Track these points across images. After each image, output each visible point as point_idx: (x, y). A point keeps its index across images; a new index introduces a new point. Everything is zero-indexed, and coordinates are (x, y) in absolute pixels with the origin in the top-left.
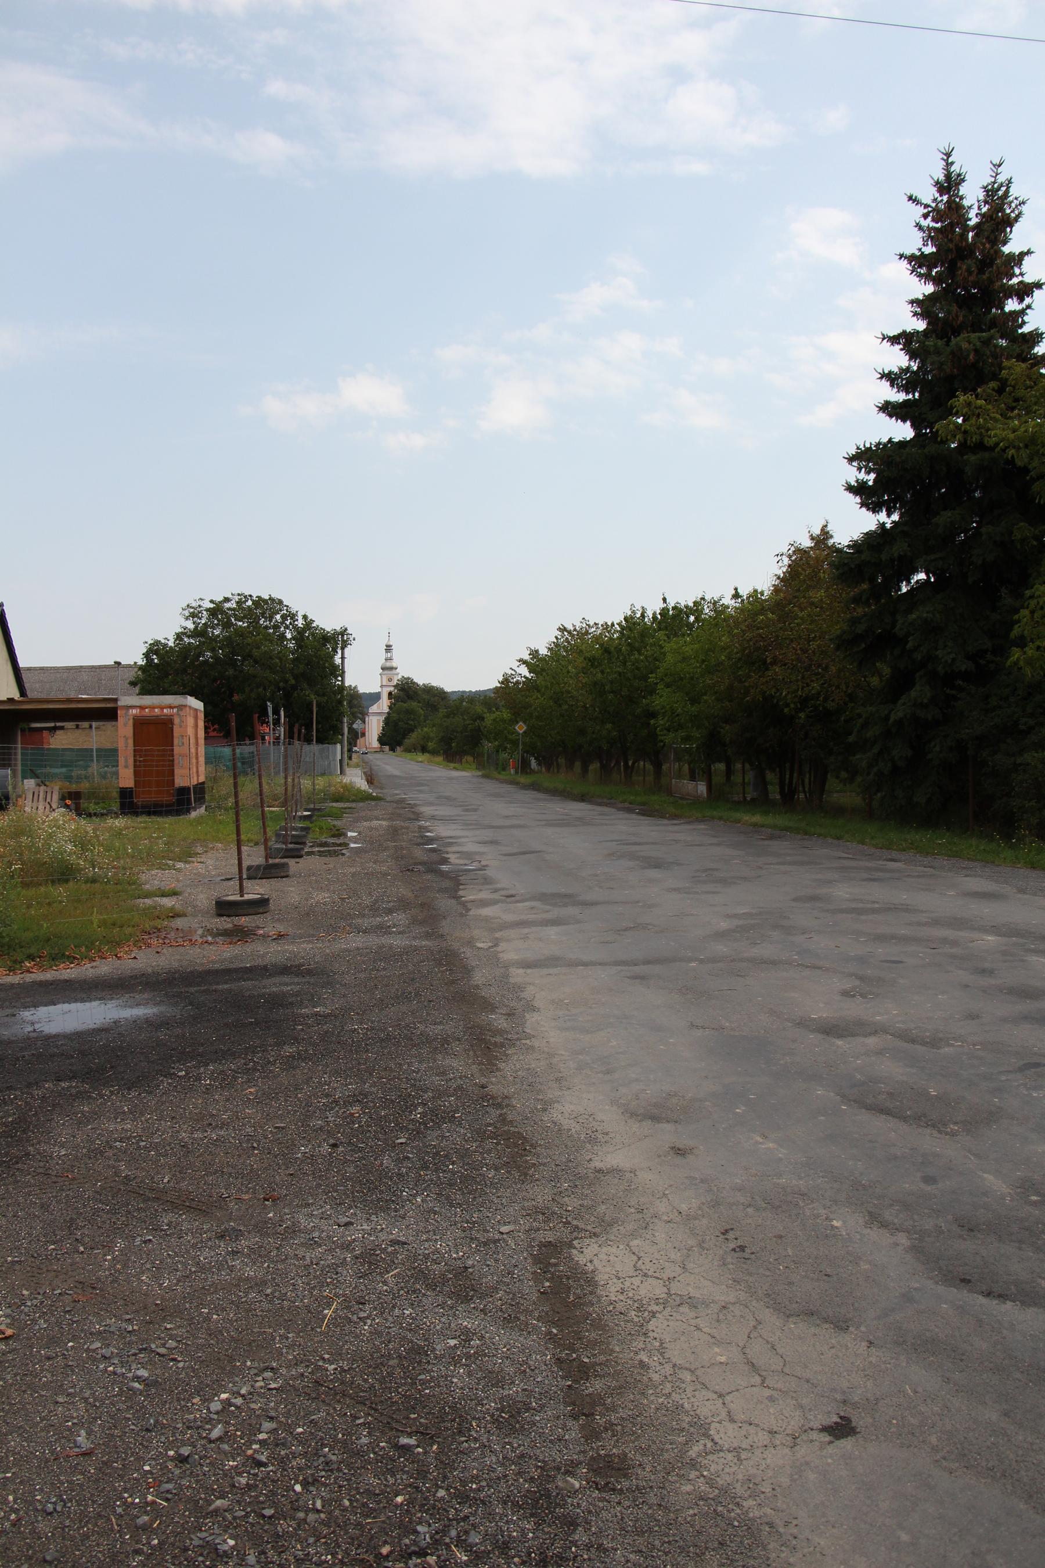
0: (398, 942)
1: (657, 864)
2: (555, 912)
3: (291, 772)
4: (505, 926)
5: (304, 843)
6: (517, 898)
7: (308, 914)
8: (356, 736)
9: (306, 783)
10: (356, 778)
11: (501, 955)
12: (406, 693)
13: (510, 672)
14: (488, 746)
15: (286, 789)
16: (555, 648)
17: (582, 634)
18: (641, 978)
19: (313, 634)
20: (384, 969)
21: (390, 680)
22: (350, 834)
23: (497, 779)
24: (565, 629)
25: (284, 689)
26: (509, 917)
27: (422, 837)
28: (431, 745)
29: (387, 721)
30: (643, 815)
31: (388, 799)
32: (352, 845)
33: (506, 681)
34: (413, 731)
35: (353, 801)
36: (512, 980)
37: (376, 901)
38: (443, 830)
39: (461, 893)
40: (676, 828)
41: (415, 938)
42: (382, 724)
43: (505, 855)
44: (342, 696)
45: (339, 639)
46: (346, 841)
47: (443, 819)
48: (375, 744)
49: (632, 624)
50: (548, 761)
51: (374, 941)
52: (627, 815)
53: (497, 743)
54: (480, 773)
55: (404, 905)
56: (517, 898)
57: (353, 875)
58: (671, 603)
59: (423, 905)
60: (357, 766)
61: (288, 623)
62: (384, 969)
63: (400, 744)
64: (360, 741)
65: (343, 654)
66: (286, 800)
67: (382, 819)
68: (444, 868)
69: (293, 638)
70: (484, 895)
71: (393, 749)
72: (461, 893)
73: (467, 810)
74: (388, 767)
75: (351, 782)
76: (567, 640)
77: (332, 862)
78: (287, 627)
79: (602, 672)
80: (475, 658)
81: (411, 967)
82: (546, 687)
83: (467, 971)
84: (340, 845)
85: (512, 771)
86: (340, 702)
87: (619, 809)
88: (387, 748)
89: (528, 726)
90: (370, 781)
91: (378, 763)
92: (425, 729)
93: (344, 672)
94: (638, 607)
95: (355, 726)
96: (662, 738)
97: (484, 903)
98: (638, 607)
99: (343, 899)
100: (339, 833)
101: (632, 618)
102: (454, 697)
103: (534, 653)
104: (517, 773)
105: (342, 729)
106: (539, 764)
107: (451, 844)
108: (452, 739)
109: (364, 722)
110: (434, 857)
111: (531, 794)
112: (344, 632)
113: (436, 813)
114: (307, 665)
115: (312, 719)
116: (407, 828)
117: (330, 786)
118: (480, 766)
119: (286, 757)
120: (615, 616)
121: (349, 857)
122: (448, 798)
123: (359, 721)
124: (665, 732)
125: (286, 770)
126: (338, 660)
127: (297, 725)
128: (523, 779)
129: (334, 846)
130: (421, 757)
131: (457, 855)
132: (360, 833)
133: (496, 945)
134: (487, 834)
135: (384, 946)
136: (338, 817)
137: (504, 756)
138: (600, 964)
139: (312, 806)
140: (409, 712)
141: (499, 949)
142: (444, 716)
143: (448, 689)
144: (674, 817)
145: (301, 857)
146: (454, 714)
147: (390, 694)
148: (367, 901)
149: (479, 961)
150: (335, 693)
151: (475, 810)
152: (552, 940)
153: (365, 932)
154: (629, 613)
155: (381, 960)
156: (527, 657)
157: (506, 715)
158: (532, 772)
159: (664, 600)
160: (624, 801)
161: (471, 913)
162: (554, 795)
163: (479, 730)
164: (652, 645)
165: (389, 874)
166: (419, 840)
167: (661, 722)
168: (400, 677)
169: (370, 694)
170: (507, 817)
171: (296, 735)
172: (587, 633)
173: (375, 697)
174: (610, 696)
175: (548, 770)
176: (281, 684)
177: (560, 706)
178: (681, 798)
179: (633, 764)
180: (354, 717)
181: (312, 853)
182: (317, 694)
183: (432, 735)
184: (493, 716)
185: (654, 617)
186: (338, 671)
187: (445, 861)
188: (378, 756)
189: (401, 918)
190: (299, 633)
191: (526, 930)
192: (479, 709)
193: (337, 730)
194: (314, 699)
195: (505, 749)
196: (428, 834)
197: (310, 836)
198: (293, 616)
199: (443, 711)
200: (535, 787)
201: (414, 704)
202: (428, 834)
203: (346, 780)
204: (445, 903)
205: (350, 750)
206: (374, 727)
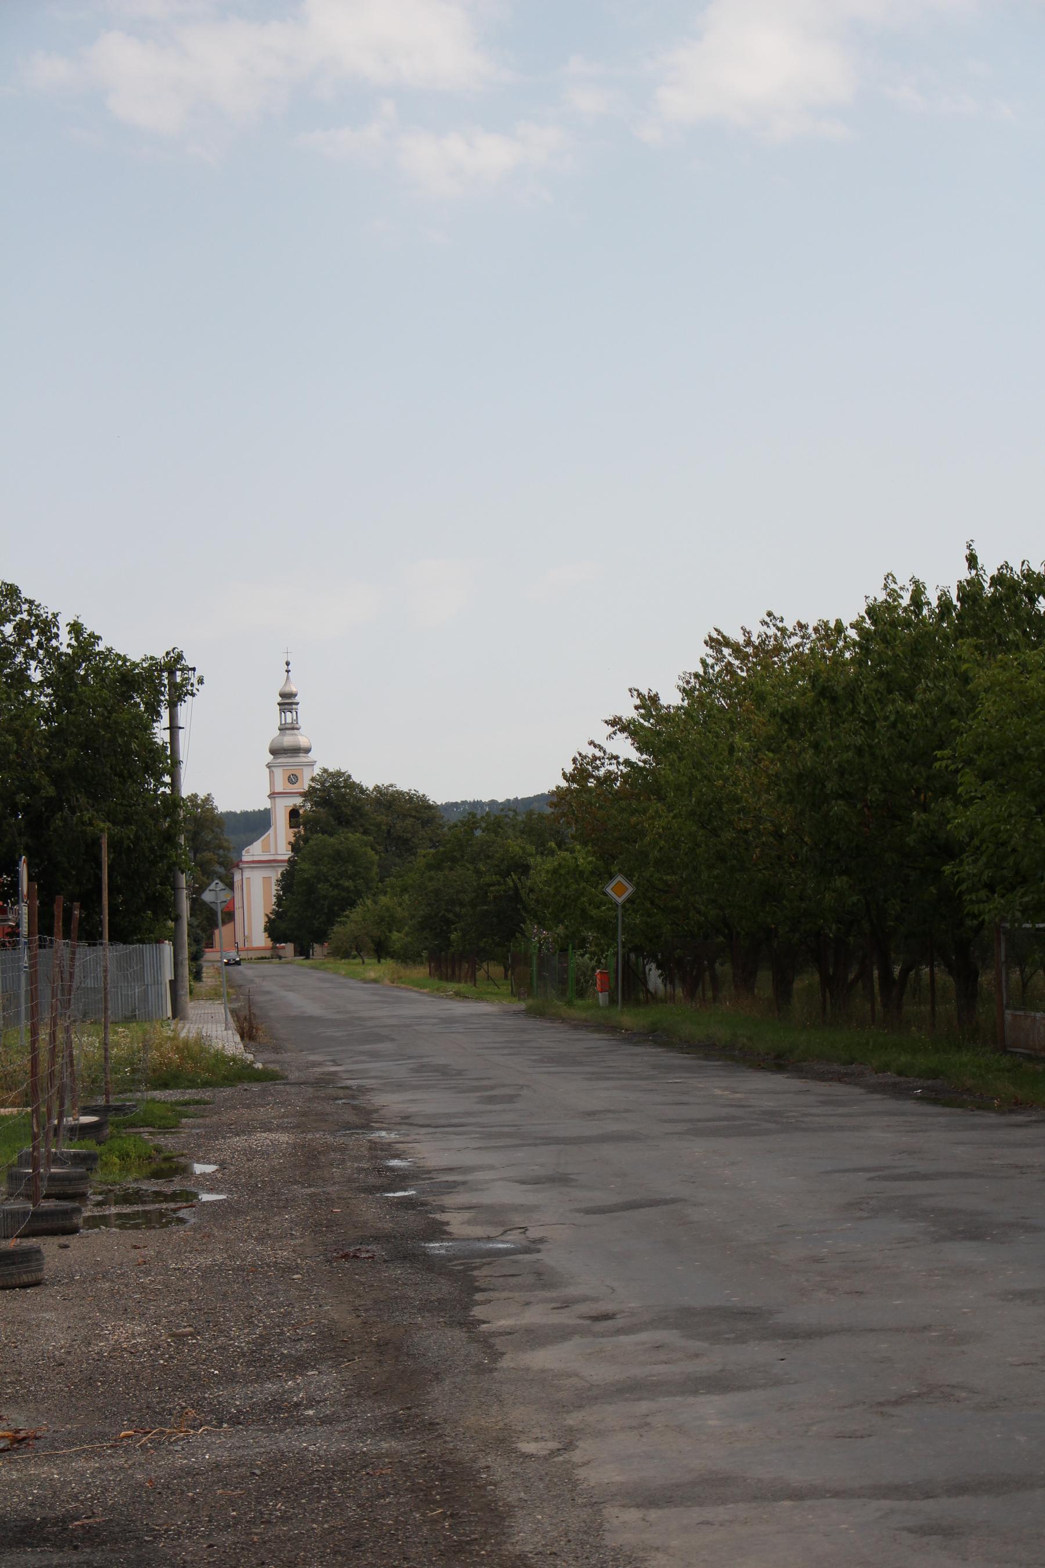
0: (317, 1444)
1: (973, 1229)
2: (716, 1358)
3: (47, 1017)
4: (590, 1396)
5: (82, 1197)
6: (620, 1322)
7: (90, 1381)
8: (209, 921)
9: (86, 1043)
10: (212, 1027)
11: (581, 1473)
12: (335, 811)
13: (590, 751)
14: (538, 936)
15: (34, 1062)
16: (701, 689)
17: (764, 653)
18: (946, 1531)
19: (97, 671)
20: (285, 1519)
21: (293, 779)
22: (199, 1168)
23: (563, 1020)
24: (727, 643)
25: (26, 808)
26: (600, 1373)
27: (381, 1170)
28: (397, 938)
29: (289, 882)
30: (935, 1101)
31: (294, 1076)
32: (206, 1197)
33: (580, 773)
34: (353, 904)
35: (206, 1084)
36: (611, 1540)
37: (265, 1339)
38: (430, 1153)
39: (478, 1312)
40: (1019, 1134)
41: (362, 1433)
42: (274, 889)
43: (588, 1211)
44: (175, 822)
45: (165, 681)
46: (189, 1186)
47: (436, 1125)
48: (260, 939)
49: (895, 632)
50: (688, 971)
51: (257, 1444)
52: (892, 1104)
53: (561, 930)
54: (522, 1006)
55: (333, 1346)
56: (620, 1322)
57: (207, 1273)
58: (990, 568)
59: (381, 1346)
60: (214, 995)
61: (33, 643)
62: (285, 1519)
63: (320, 937)
64: (222, 934)
65: (173, 717)
66: (34, 1088)
67: (281, 1128)
68: (435, 1247)
69: (47, 682)
70: (535, 1316)
71: (303, 951)
72: (478, 1312)
73: (491, 1100)
74: (292, 997)
75: (200, 1038)
76: (729, 668)
77: (151, 1240)
78: (31, 654)
79: (816, 746)
80: (503, 703)
81: (352, 1511)
82: (678, 788)
83: (497, 1516)
84: (173, 1197)
85: (602, 998)
86: (169, 838)
87: (873, 1089)
88: (289, 948)
89: (637, 885)
90: (248, 1033)
91: (268, 986)
92: (384, 900)
93: (176, 763)
94: (903, 580)
95: (207, 897)
96: (976, 909)
97: (536, 1337)
98: (903, 580)
99: (180, 1338)
100: (171, 1168)
101: (889, 608)
102: (454, 818)
103: (649, 703)
104: (613, 1001)
105: (176, 904)
106: (668, 978)
107: (451, 1187)
108: (448, 922)
109: (230, 885)
110: (410, 1220)
111: (649, 1055)
112: (174, 662)
113: (413, 1109)
114: (84, 747)
115: (99, 880)
116: (343, 1149)
117: (146, 1047)
118: (521, 988)
119: (32, 979)
120: (848, 609)
121: (196, 1229)
122: (443, 1071)
123: (217, 885)
124: (983, 893)
125: (34, 1013)
126: (161, 734)
127: (60, 899)
128: (628, 1018)
129: (158, 1199)
130: (374, 969)
131: (467, 1215)
132: (223, 1165)
133: (569, 1447)
134: (541, 1160)
135: (283, 1457)
136: (167, 1127)
137: (580, 960)
138: (836, 1494)
139: (101, 1101)
140: (340, 857)
141: (576, 1456)
142: (429, 867)
143: (438, 796)
144: (1015, 1105)
145: (73, 1231)
146: (454, 860)
147: (294, 813)
148: (242, 1340)
149: (527, 1489)
150: (154, 814)
151: (511, 1099)
152: (709, 1431)
153: (235, 1421)
154: (882, 596)
155: (277, 1495)
156: (629, 711)
157: (583, 858)
158: (652, 998)
159: (972, 560)
160: (884, 1068)
161: (505, 1363)
162: (706, 1057)
163: (515, 897)
164: (941, 675)
165: (296, 1269)
166: (372, 1180)
167: (969, 869)
168: (317, 771)
169: (245, 814)
170: (591, 1114)
171: (58, 925)
172: (779, 649)
173: (256, 823)
174: (838, 807)
175: (691, 994)
176: (22, 798)
177: (715, 833)
178: (1029, 1058)
179: (905, 972)
180: (205, 874)
181: (104, 1220)
182: (110, 817)
183: (400, 913)
184: (550, 863)
185: (945, 605)
186: (164, 761)
187: (438, 1231)
188: (266, 968)
189: (325, 1381)
190: (62, 667)
191: (644, 1406)
192: (515, 845)
193: (163, 906)
194: (104, 830)
195: (582, 943)
196: (395, 1163)
197: (97, 1176)
198: (46, 627)
199: (425, 853)
200: (657, 1036)
201: (353, 838)
202: (395, 1163)
203: (187, 1031)
204: (438, 1340)
205: (195, 957)
206: (256, 895)
